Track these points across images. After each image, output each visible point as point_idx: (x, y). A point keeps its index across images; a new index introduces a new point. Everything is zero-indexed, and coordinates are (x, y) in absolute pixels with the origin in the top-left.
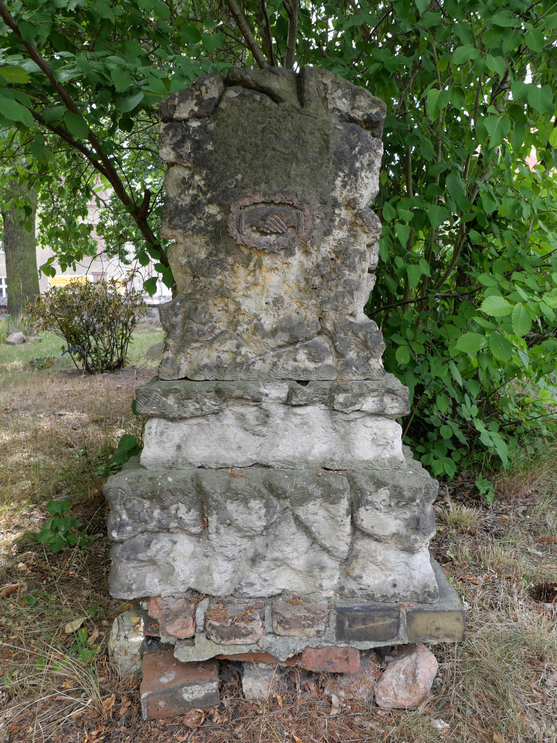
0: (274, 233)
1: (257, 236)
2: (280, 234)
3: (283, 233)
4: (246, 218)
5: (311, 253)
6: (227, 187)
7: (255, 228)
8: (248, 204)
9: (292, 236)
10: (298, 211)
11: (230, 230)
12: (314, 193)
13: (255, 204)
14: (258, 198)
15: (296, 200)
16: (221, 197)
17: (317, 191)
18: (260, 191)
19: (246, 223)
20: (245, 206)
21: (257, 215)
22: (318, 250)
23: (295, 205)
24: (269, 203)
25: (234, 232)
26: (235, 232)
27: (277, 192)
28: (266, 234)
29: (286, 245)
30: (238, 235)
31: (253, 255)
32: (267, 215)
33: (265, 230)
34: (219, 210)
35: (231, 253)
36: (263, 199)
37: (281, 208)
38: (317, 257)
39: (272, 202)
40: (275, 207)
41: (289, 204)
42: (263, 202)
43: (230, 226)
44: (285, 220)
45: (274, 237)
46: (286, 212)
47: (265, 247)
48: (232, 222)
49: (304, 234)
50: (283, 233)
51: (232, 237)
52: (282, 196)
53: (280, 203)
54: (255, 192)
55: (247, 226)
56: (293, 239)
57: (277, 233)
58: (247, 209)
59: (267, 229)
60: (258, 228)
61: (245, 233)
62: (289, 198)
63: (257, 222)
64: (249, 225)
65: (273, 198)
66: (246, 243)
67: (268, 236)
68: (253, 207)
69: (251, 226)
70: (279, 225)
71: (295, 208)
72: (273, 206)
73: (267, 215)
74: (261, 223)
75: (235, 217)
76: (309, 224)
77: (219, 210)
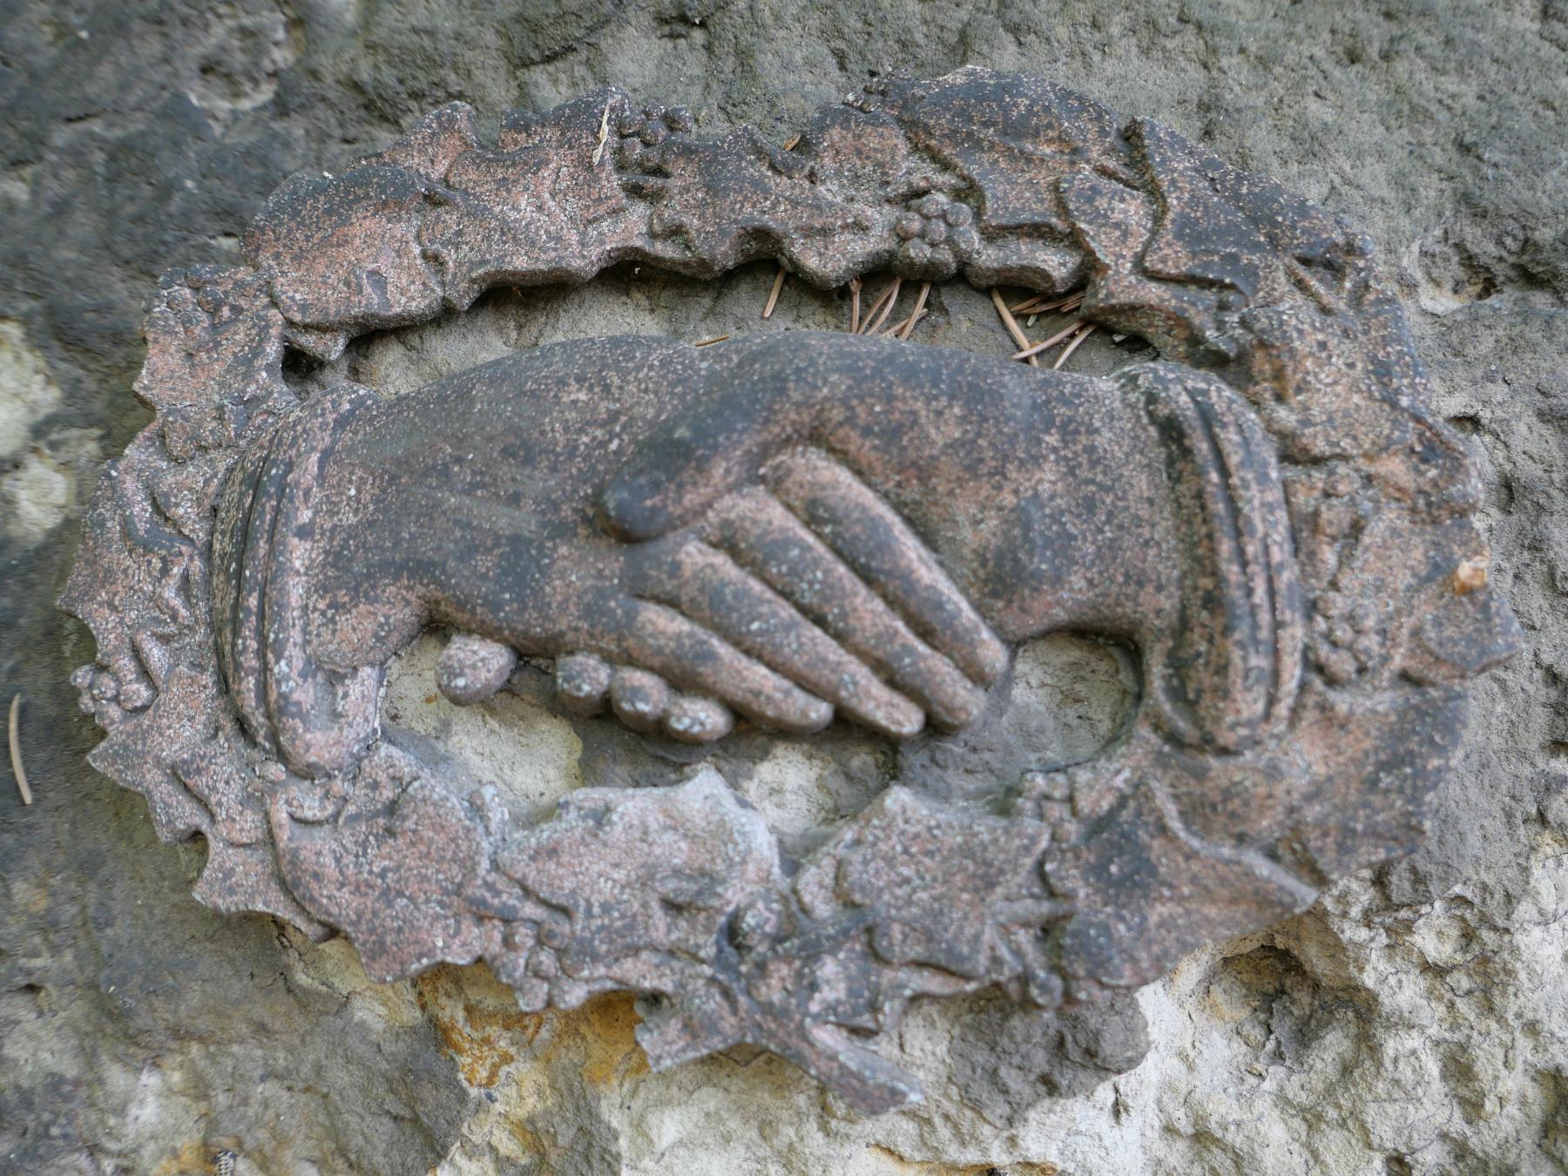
0: (786, 732)
1: (519, 767)
2: (885, 742)
3: (936, 728)
4: (354, 501)
5: (1364, 1011)
6: (176, 112)
7: (483, 661)
8: (408, 294)
9: (1102, 784)
10: (1182, 386)
11: (106, 693)
12: (1366, 129)
13: (514, 296)
14: (555, 217)
15: (1132, 209)
16: (83, 224)
17: (1405, 109)
18: (576, 119)
19: (345, 578)
20: (368, 336)
21: (523, 451)
22: (1485, 971)
23: (1121, 285)
24: (726, 281)
25: (156, 721)
26: (183, 727)
27: (829, 116)
28: (658, 749)
29: (997, 937)
30: (225, 776)
31: (472, 1068)
32: (671, 455)
33: (647, 694)
34: (48, 398)
35: (155, 1016)
36: (632, 228)
37: (885, 336)
38: (1459, 1068)
39: (762, 261)
40: (816, 335)
41: (1019, 288)
42: (627, 274)
43: (106, 626)
44: (976, 525)
45: (789, 782)
46: (978, 397)
47: (642, 973)
48: (137, 573)
49: (1306, 758)
50: (936, 728)
51: (127, 804)
52: (911, 170)
53: (878, 274)
54: (505, 150)
55: (357, 626)
56: (1115, 842)
57: (847, 726)
58: (394, 374)
59: (683, 682)
60: (534, 657)
61: (318, 743)
62: (1014, 193)
63: (522, 564)
64: (397, 607)
65: (775, 205)
66: (341, 903)
67: (704, 787)
68: (484, 346)
69: (436, 626)
70: (870, 612)
71: (1123, 334)
72: (762, 320)
73: (671, 455)
74: (576, 573)
75: (190, 488)
76: (1379, 582)
77: (48, 398)
